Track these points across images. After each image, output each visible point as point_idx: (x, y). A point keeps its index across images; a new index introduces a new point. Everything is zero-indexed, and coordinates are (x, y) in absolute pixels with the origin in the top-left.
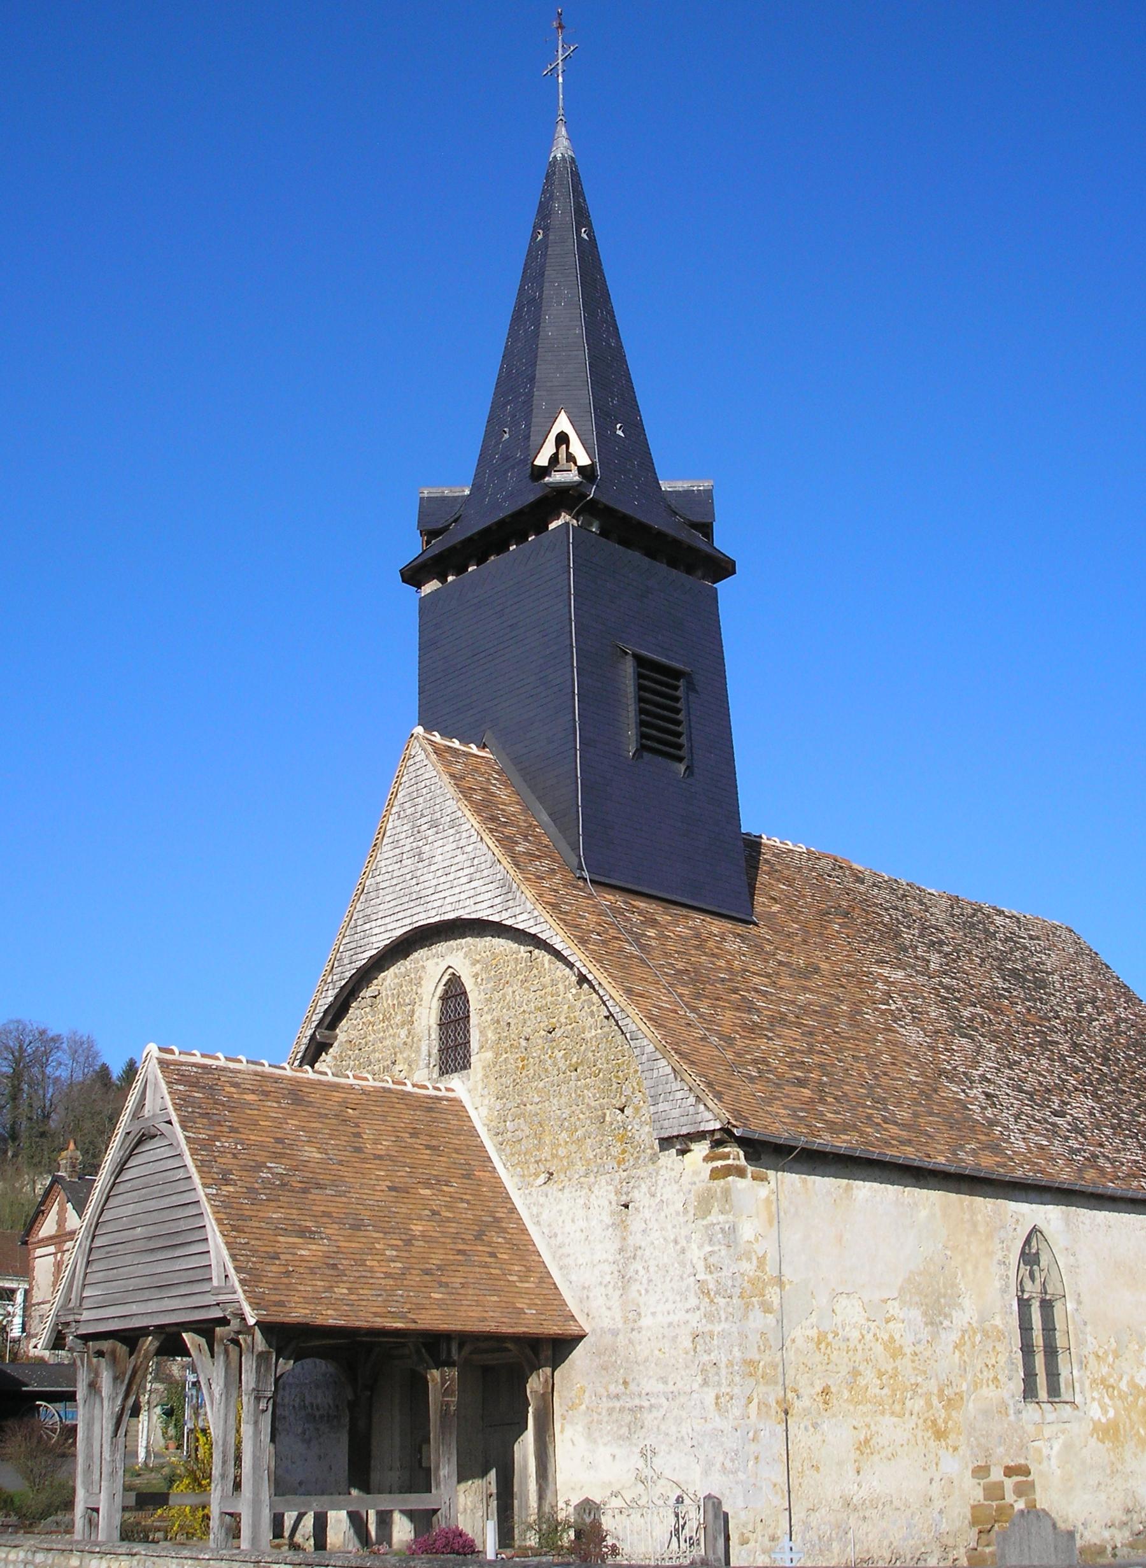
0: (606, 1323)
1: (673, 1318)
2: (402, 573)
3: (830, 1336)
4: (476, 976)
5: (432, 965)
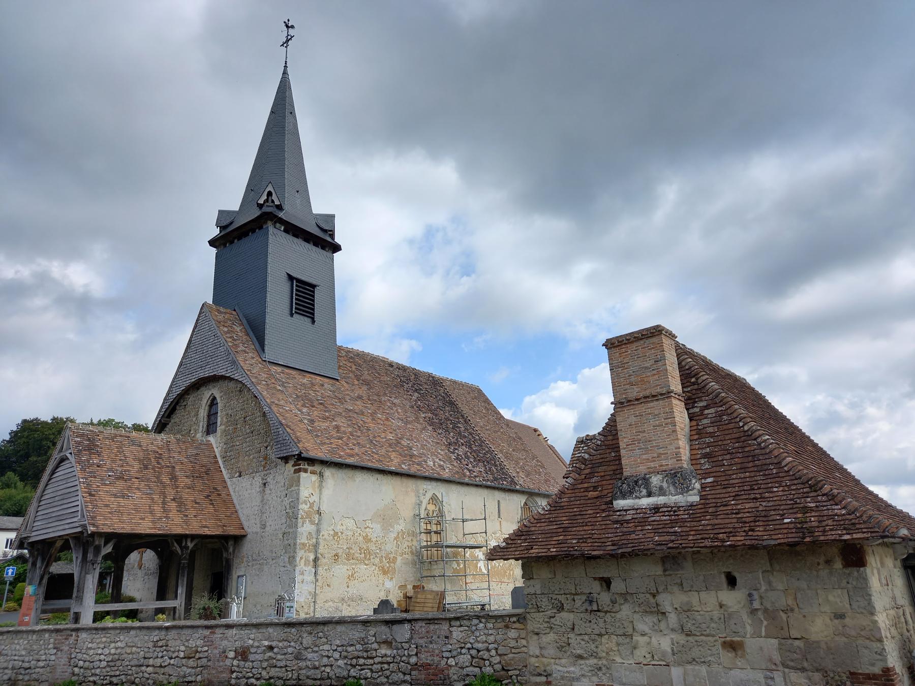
0: (255, 530)
5: (206, 394)
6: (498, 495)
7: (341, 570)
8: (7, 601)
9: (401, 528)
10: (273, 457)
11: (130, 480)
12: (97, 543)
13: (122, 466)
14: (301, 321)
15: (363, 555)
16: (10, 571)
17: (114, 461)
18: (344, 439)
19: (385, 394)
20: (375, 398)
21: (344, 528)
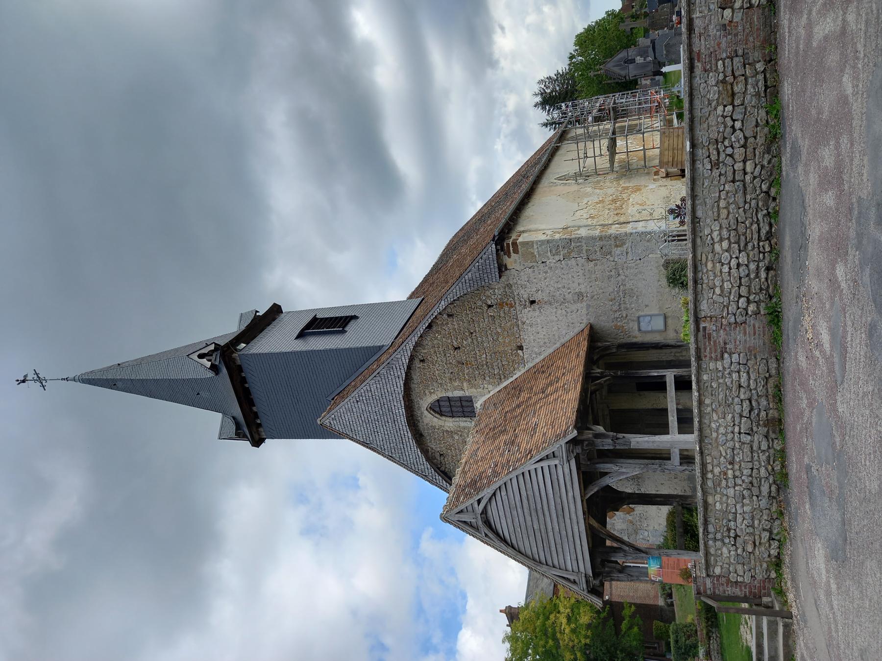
0: (584, 311)
4: (431, 393)
5: (429, 420)
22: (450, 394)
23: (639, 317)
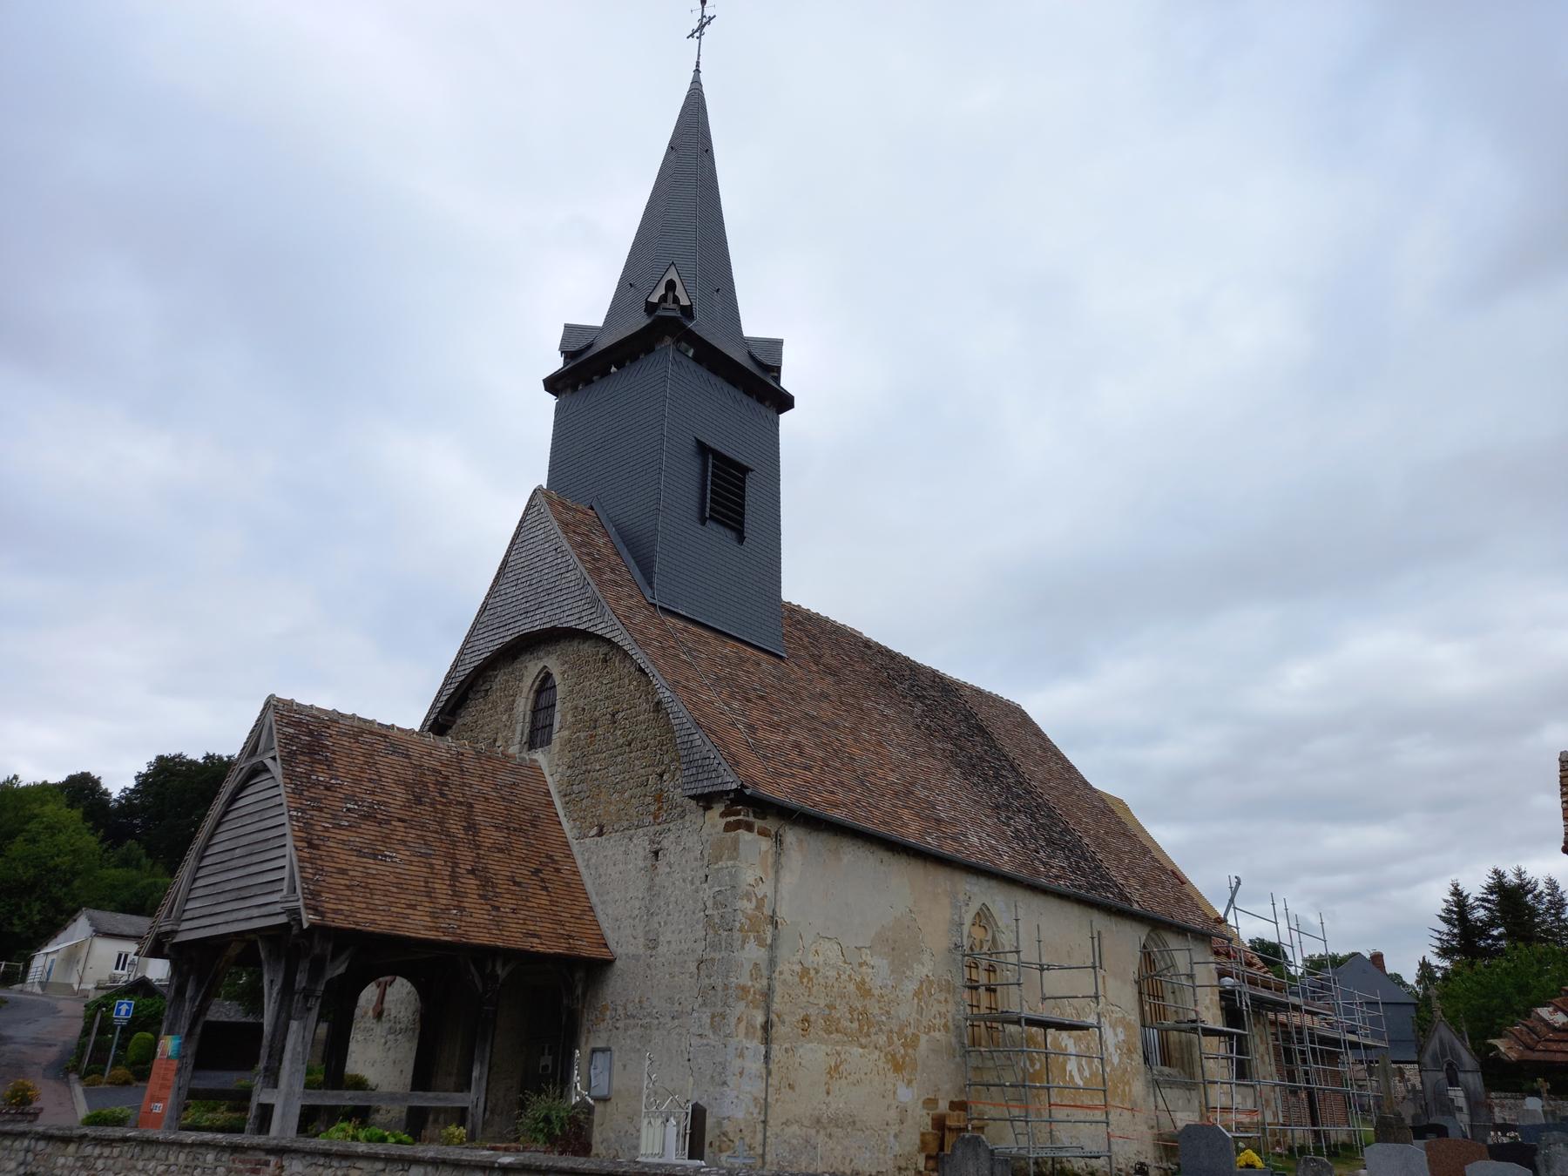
0: (632, 950)
1: (684, 947)
2: (545, 381)
3: (812, 972)
5: (531, 669)
6: (1100, 921)
7: (814, 1054)
8: (113, 1066)
9: (925, 971)
10: (677, 795)
11: (388, 822)
12: (317, 951)
13: (373, 793)
14: (718, 535)
15: (855, 1025)
16: (124, 1008)
17: (357, 781)
18: (815, 770)
19: (867, 697)
20: (851, 700)
21: (821, 959)
22: (557, 708)
23: (609, 1049)
